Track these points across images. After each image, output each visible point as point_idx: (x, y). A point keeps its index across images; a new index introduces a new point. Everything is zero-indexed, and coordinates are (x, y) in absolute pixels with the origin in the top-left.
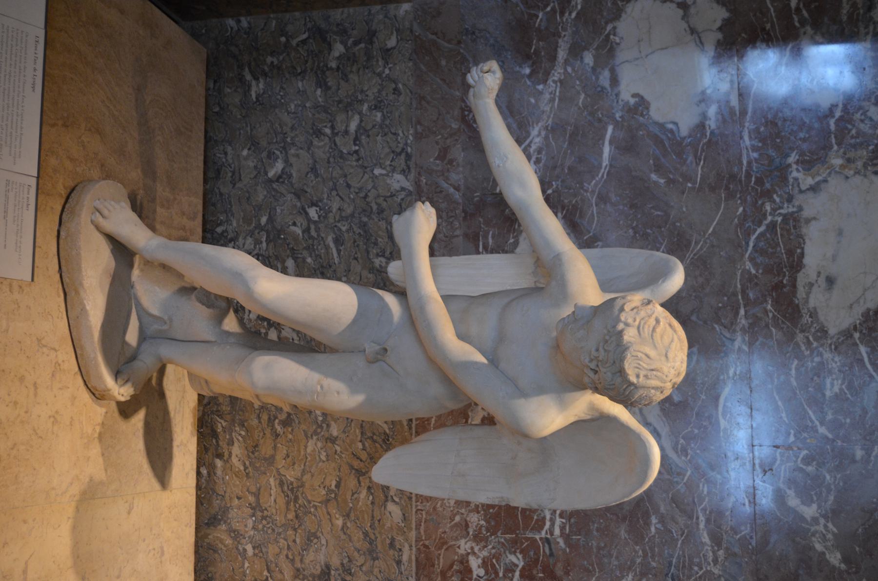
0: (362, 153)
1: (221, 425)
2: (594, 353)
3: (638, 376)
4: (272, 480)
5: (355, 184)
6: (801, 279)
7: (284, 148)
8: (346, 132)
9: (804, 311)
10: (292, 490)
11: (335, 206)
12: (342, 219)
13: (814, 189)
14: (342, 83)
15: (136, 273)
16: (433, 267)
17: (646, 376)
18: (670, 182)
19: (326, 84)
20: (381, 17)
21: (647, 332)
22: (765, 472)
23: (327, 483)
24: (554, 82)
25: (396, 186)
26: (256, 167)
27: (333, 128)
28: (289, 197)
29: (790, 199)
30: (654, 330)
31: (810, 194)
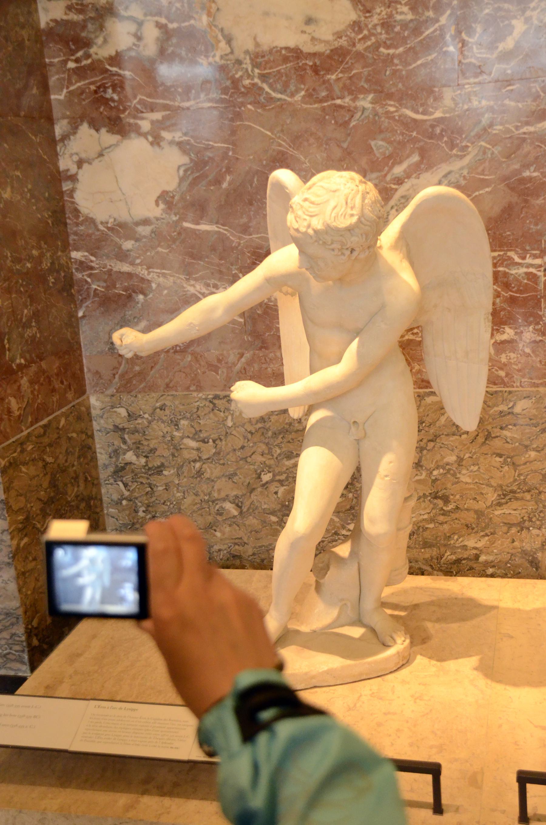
1: (449, 556)
2: (336, 252)
3: (352, 215)
4: (497, 513)
5: (240, 443)
6: (308, 48)
8: (198, 449)
9: (336, 44)
11: (259, 458)
12: (270, 453)
13: (229, 40)
14: (157, 453)
15: (304, 629)
16: (294, 380)
17: (352, 208)
18: (228, 171)
19: (159, 467)
20: (102, 421)
21: (314, 209)
22: (482, 72)
23: (498, 465)
24: (149, 273)
26: (230, 525)
27: (195, 461)
29: (239, 62)
30: (312, 203)
31: (234, 43)
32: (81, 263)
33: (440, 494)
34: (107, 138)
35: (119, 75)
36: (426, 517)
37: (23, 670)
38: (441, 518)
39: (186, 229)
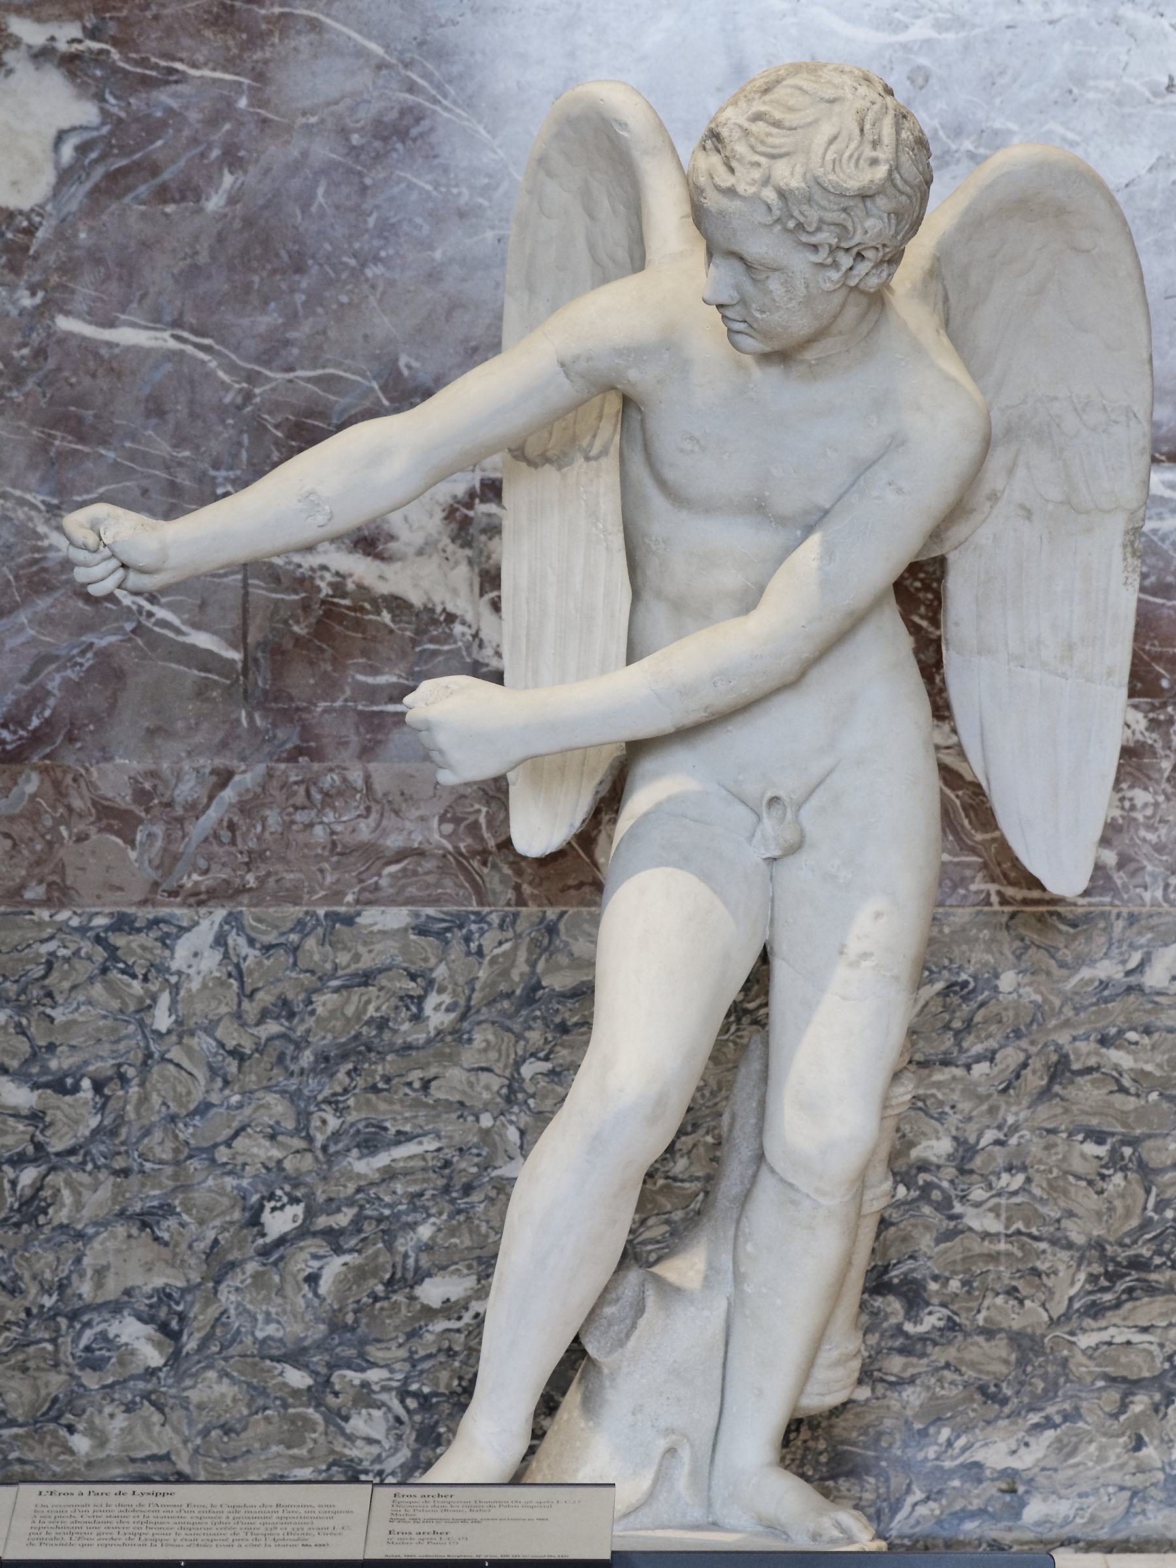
0: (104, 1067)
4: (1085, 1341)
7: (73, 1316)
8: (35, 1117)
10: (1113, 1277)
12: (303, 1129)
17: (875, 144)
18: (232, 159)
21: (779, 140)
25: (211, 961)
26: (129, 1408)
27: (19, 1161)
28: (227, 1296)
30: (777, 124)
33: (895, 1275)
38: (895, 1364)
39: (66, 338)
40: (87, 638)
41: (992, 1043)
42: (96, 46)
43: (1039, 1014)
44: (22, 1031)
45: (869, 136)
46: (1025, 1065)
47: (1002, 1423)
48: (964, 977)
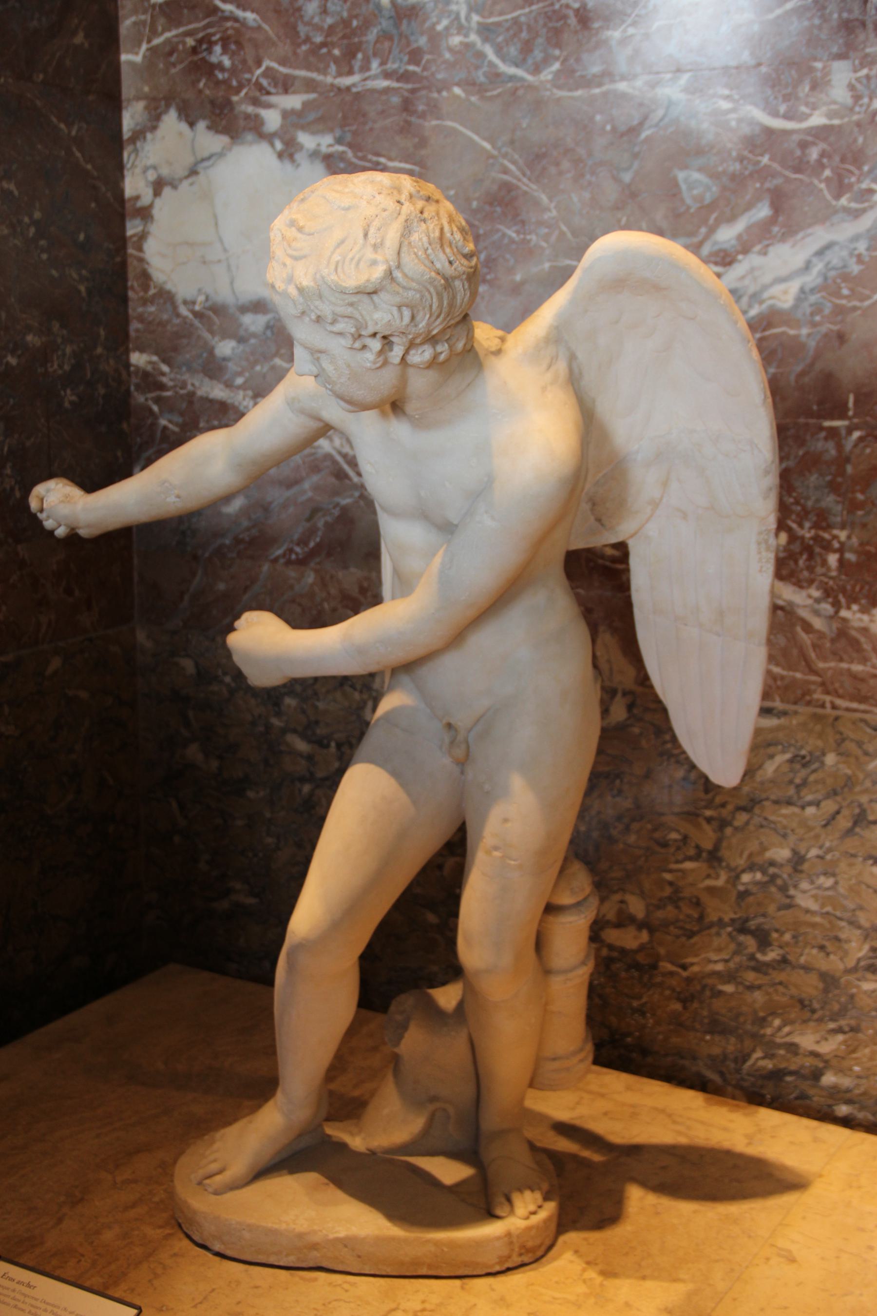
8: (310, 758)
15: (357, 1143)
27: (302, 780)
32: (146, 375)
33: (752, 924)
34: (208, 140)
35: (236, 20)
36: (719, 967)
37: (333, 1086)
38: (751, 977)
40: (337, 499)
41: (819, 796)
42: (340, 148)
43: (849, 783)
44: (304, 712)
45: (372, 240)
46: (838, 812)
47: (812, 1024)
48: (803, 752)
